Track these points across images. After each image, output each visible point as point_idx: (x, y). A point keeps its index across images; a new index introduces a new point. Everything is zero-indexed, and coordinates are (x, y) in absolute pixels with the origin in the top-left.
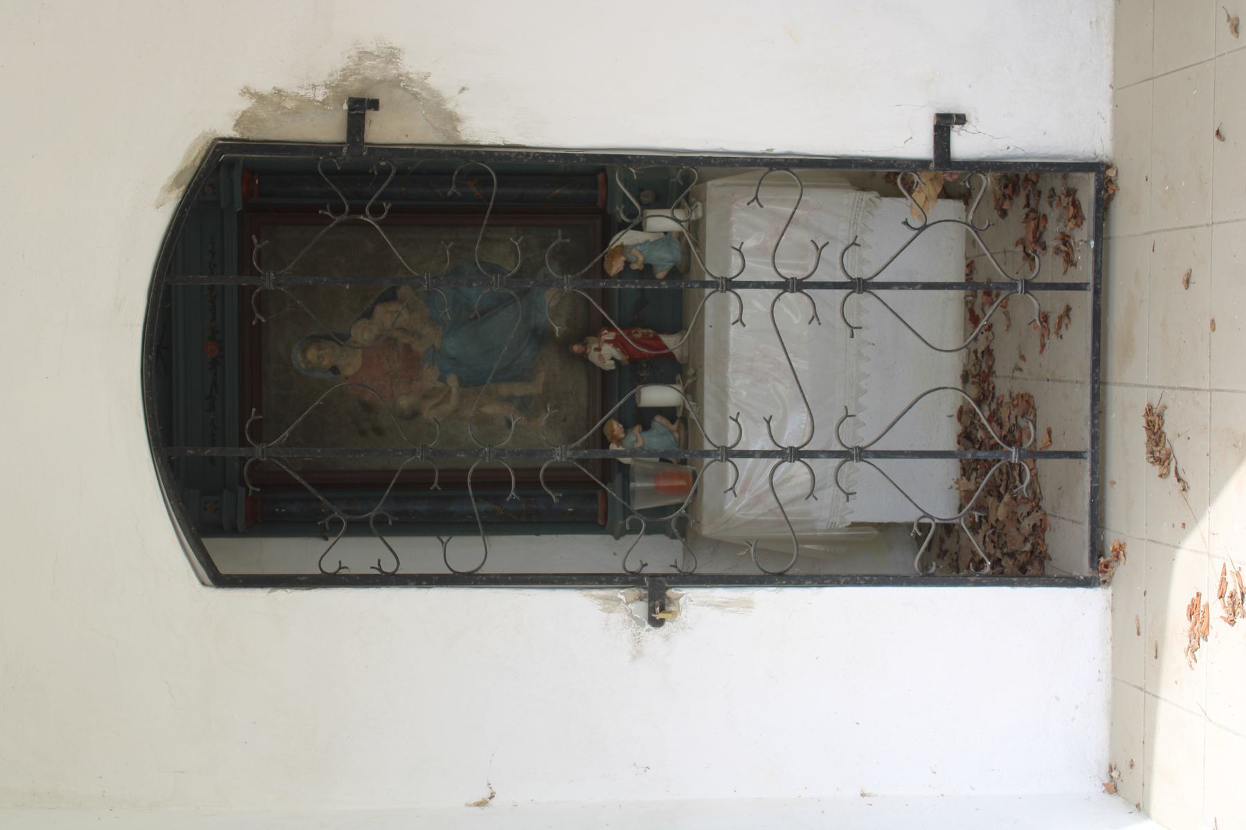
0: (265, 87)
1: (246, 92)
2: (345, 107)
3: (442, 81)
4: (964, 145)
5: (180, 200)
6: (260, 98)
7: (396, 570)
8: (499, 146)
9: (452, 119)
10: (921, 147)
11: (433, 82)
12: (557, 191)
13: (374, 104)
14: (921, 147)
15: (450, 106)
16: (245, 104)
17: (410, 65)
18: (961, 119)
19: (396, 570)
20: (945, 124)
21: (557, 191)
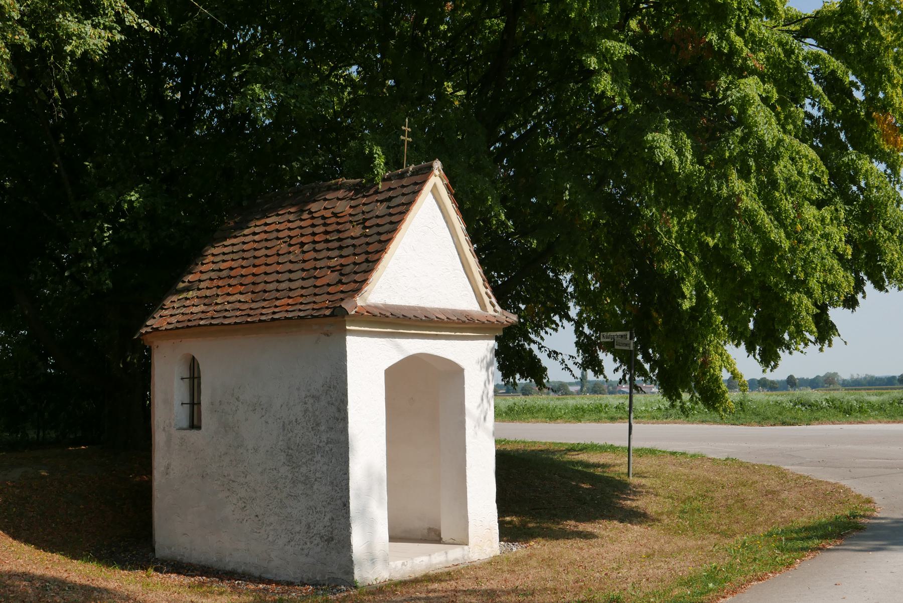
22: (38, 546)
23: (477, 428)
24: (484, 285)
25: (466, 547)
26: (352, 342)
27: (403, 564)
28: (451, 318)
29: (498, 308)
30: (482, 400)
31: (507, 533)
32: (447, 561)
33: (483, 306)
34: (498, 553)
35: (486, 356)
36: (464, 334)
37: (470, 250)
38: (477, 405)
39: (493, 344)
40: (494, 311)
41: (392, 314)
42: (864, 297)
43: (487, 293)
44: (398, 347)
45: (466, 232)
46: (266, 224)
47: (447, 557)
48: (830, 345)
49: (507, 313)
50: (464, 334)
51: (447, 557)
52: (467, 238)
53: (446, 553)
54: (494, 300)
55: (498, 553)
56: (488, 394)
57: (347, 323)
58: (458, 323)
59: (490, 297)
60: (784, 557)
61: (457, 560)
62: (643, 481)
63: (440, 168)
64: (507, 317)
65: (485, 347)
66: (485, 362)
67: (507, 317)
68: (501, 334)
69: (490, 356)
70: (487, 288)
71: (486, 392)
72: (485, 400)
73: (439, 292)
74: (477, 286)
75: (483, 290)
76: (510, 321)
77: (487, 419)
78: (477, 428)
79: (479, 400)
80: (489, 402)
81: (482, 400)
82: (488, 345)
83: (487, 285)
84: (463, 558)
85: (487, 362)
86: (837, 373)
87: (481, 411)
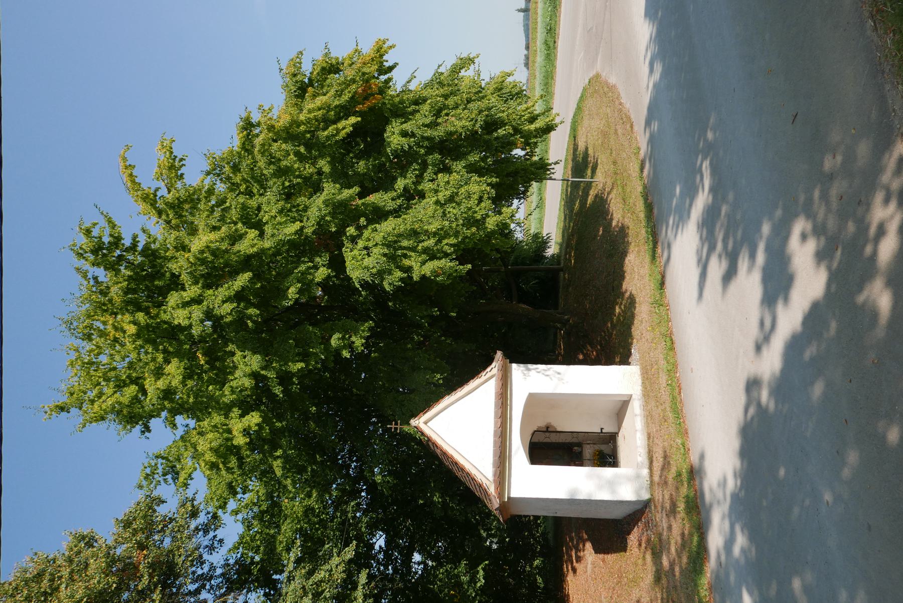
3: (555, 425)
4: (603, 431)
17: (552, 424)
20: (602, 429)
22: (567, 365)
25: (634, 397)
26: (513, 494)
27: (640, 455)
30: (547, 375)
31: (625, 361)
32: (641, 416)
33: (492, 377)
34: (638, 367)
35: (522, 370)
39: (514, 366)
40: (494, 369)
42: (387, 61)
48: (467, 62)
49: (496, 359)
55: (638, 367)
56: (544, 370)
58: (503, 408)
60: (340, 196)
61: (640, 405)
65: (517, 370)
66: (525, 372)
68: (508, 360)
71: (543, 372)
72: (547, 373)
76: (501, 358)
77: (559, 371)
79: (548, 378)
80: (549, 369)
81: (547, 375)
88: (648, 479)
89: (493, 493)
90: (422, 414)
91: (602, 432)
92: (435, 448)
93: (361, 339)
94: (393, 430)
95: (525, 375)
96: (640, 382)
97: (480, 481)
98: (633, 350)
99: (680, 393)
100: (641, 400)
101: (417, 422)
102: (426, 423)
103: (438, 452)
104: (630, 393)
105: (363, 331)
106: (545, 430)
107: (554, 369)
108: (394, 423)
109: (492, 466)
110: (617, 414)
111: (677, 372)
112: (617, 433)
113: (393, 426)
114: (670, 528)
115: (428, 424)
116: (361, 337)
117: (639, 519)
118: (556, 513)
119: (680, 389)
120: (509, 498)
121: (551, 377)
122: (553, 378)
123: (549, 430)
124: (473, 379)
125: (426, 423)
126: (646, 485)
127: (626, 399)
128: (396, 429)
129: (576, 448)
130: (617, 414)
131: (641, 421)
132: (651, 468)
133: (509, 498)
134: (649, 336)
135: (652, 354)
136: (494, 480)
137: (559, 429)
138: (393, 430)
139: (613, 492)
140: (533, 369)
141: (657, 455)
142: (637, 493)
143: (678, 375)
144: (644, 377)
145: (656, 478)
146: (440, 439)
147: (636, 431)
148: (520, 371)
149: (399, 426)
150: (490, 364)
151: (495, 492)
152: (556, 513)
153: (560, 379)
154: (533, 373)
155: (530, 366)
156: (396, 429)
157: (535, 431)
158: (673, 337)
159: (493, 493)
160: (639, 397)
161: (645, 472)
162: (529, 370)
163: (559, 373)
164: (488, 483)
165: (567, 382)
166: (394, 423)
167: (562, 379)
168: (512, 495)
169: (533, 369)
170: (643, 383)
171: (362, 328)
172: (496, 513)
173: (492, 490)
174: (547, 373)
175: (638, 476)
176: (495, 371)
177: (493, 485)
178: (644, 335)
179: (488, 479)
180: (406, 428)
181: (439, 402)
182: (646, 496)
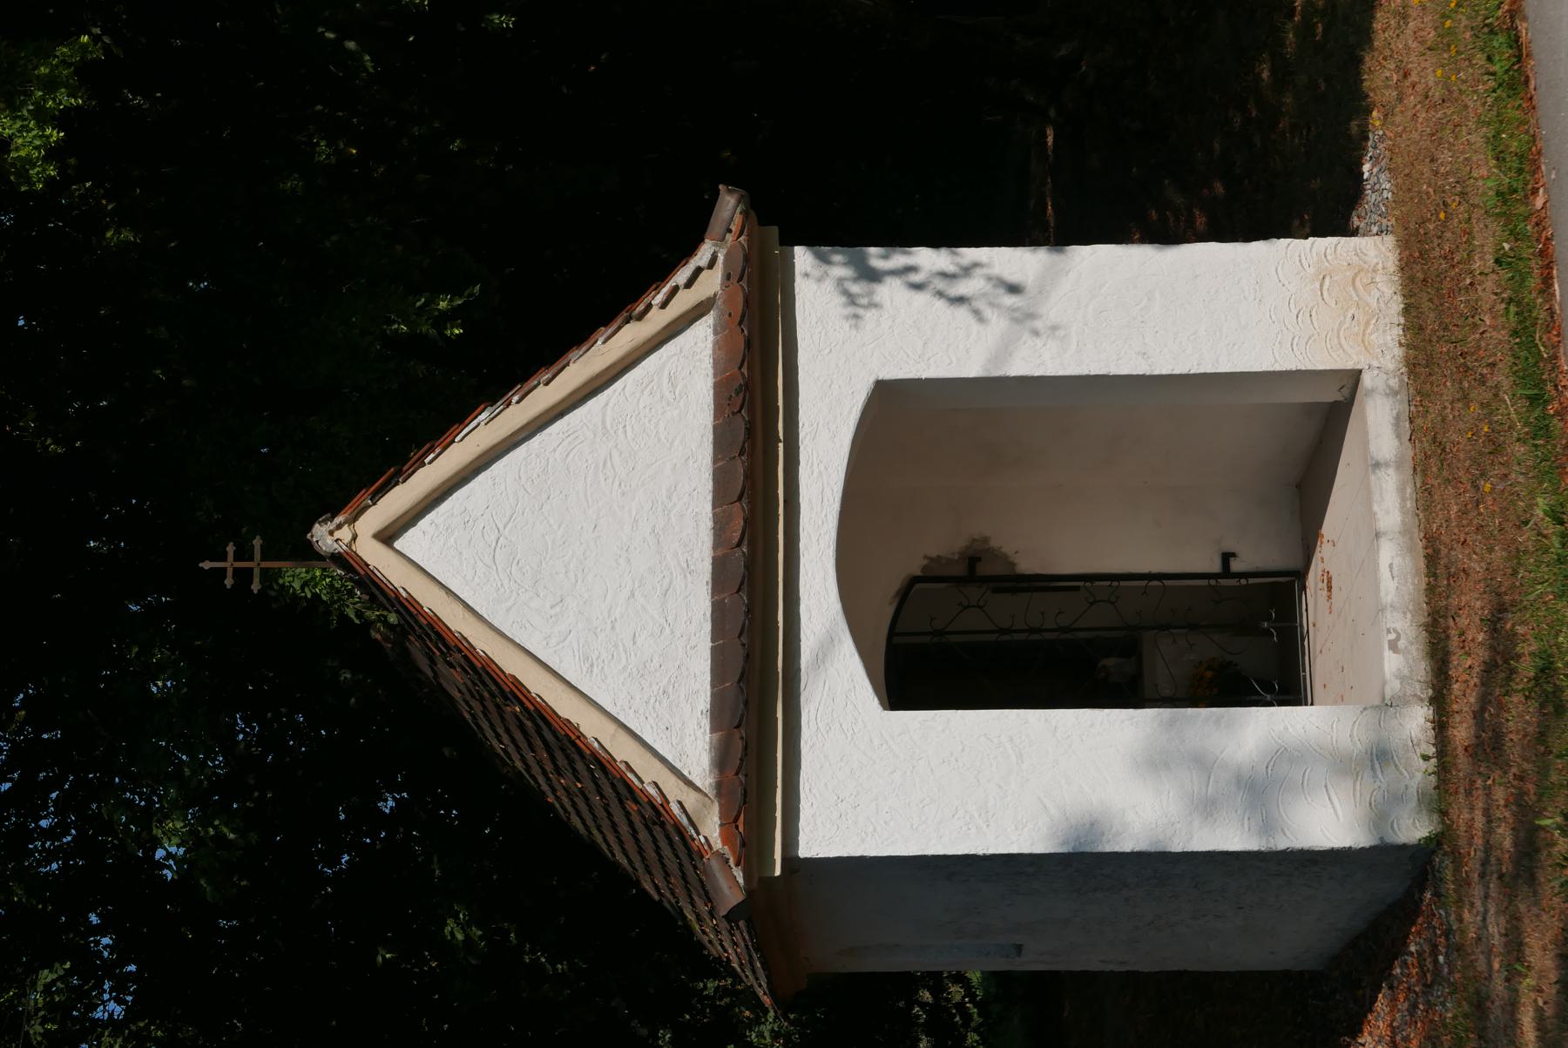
0: (934, 554)
1: (926, 557)
2: (967, 561)
3: (1008, 549)
4: (1236, 566)
5: (895, 605)
6: (931, 559)
7: (1042, 625)
8: (381, 497)
9: (1013, 565)
10: (1215, 567)
11: (1003, 550)
12: (1050, 208)
13: (979, 559)
14: (1215, 567)
15: (1011, 560)
16: (926, 562)
17: (994, 544)
18: (1233, 555)
19: (1042, 625)
20: (1227, 557)
21: (1050, 208)
23: (1038, 324)
24: (640, 317)
25: (1367, 380)
26: (811, 846)
27: (1393, 646)
28: (740, 488)
29: (702, 256)
30: (960, 300)
32: (1399, 465)
34: (1390, 240)
35: (840, 281)
36: (780, 403)
37: (547, 384)
38: (975, 327)
41: (737, 727)
43: (664, 305)
44: (820, 659)
45: (499, 406)
46: (528, 768)
47: (1387, 465)
50: (780, 403)
51: (1387, 465)
52: (516, 398)
53: (1377, 465)
54: (681, 276)
55: (1390, 240)
56: (944, 275)
57: (766, 875)
59: (675, 290)
61: (1397, 418)
62: (1195, 792)
63: (331, 526)
64: (730, 231)
66: (855, 288)
67: (730, 231)
69: (839, 268)
70: (649, 307)
71: (940, 284)
72: (962, 288)
73: (670, 498)
74: (644, 344)
75: (657, 319)
76: (738, 219)
77: (1013, 277)
78: (1038, 324)
79: (962, 312)
80: (967, 271)
81: (960, 300)
82: (806, 275)
83: (641, 307)
84: (1396, 393)
85: (855, 280)
86: (885, 709)
87: (992, 305)
88: (1432, 750)
89: (717, 845)
90: (364, 497)
91: (1226, 572)
92: (441, 666)
93: (41, 125)
94: (229, 582)
95: (852, 299)
96: (1397, 305)
97: (652, 791)
98: (1366, 167)
99: (1547, 281)
100: (1403, 396)
101: (345, 534)
102: (388, 537)
103: (454, 681)
104: (1349, 365)
105: (50, 85)
106: (960, 570)
107: (996, 270)
108: (231, 549)
109: (706, 723)
110: (1299, 486)
111: (1535, 192)
112: (1300, 575)
113: (229, 564)
114: (1515, 946)
115: (397, 545)
116: (42, 117)
117: (1397, 949)
118: (1019, 949)
119: (1549, 267)
120: (792, 861)
121: (980, 304)
122: (988, 313)
123: (984, 569)
124: (606, 324)
125: (388, 537)
126: (1419, 776)
127: (1331, 395)
128: (244, 576)
129: (1110, 662)
130: (1299, 486)
131: (1401, 490)
132: (1440, 700)
133: (790, 860)
134: (1429, 74)
135: (1445, 156)
136: (720, 787)
137: (1028, 565)
138: (229, 582)
139: (1267, 827)
140: (894, 273)
141: (1463, 622)
142: (1379, 816)
143: (1539, 202)
144: (1412, 279)
145: (1462, 733)
146: (459, 609)
147: (1377, 535)
148: (829, 285)
149: (256, 564)
150: (690, 250)
151: (726, 840)
152: (1019, 949)
153: (1024, 318)
154: (890, 292)
155: (875, 256)
156: (244, 576)
157: (914, 581)
158: (1522, 27)
159: (717, 845)
160: (1394, 382)
161: (1416, 722)
162: (872, 276)
163: (1014, 289)
164: (691, 799)
165: (1054, 328)
166: (231, 549)
167: (1031, 316)
168: (806, 849)
169: (894, 273)
170: (1406, 311)
171: (43, 70)
172: (731, 948)
173: (711, 829)
174: (962, 288)
175: (1380, 756)
176: (711, 283)
177: (716, 808)
178: (1414, 78)
179: (689, 783)
180: (294, 576)
181: (446, 438)
182: (1413, 829)
